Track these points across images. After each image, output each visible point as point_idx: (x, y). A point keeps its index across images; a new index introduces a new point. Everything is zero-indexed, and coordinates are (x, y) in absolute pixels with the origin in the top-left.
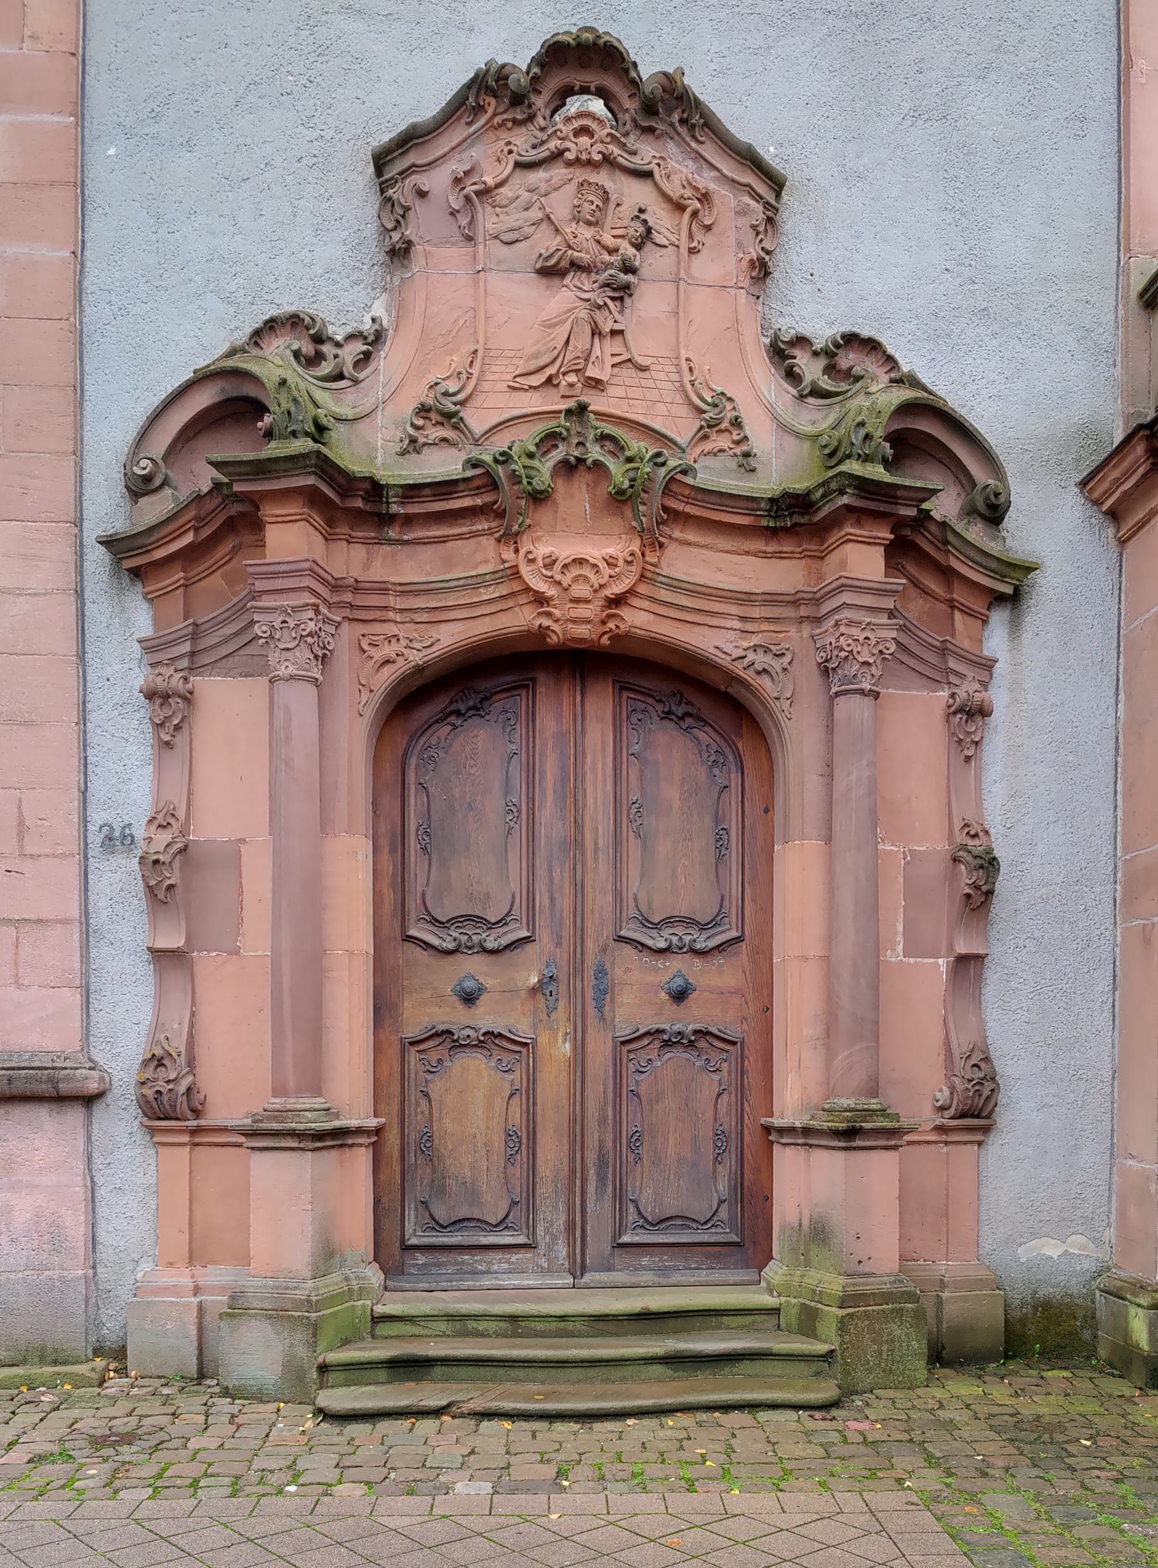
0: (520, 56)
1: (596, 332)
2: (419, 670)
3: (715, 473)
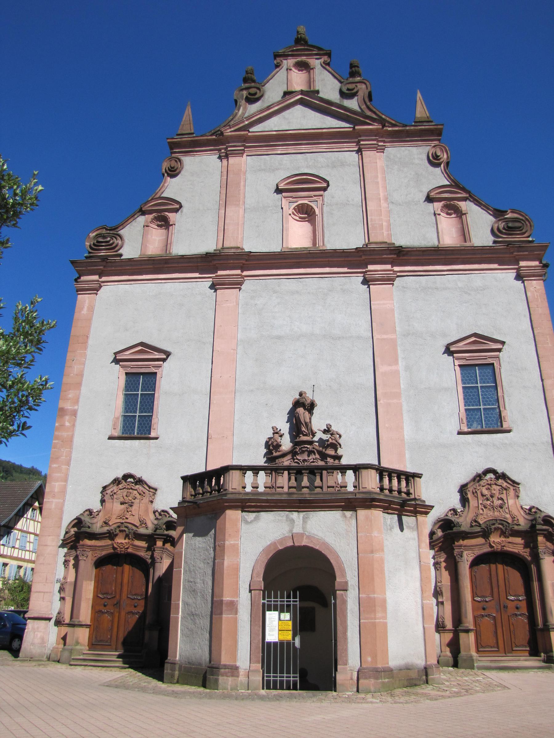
0: (120, 475)
1: (128, 511)
2: (100, 557)
3: (142, 531)
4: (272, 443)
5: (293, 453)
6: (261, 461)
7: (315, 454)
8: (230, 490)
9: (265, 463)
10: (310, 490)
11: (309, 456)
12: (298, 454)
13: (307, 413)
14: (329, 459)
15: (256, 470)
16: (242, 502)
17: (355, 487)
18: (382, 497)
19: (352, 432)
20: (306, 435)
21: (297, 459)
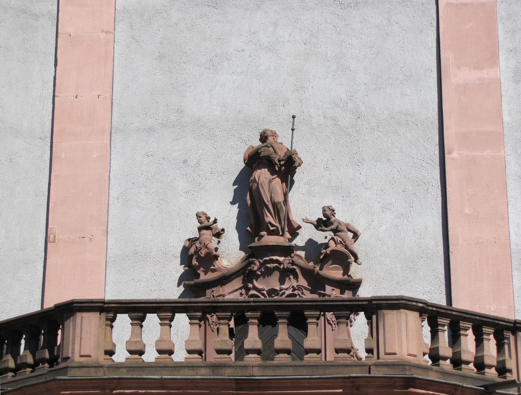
4: (196, 252)
5: (245, 274)
6: (173, 292)
7: (296, 277)
8: (77, 358)
9: (179, 297)
10: (264, 359)
11: (282, 281)
12: (257, 277)
13: (278, 180)
14: (329, 289)
15: (166, 310)
16: (103, 388)
17: (369, 351)
18: (432, 376)
19: (384, 227)
20: (275, 233)
21: (255, 288)
